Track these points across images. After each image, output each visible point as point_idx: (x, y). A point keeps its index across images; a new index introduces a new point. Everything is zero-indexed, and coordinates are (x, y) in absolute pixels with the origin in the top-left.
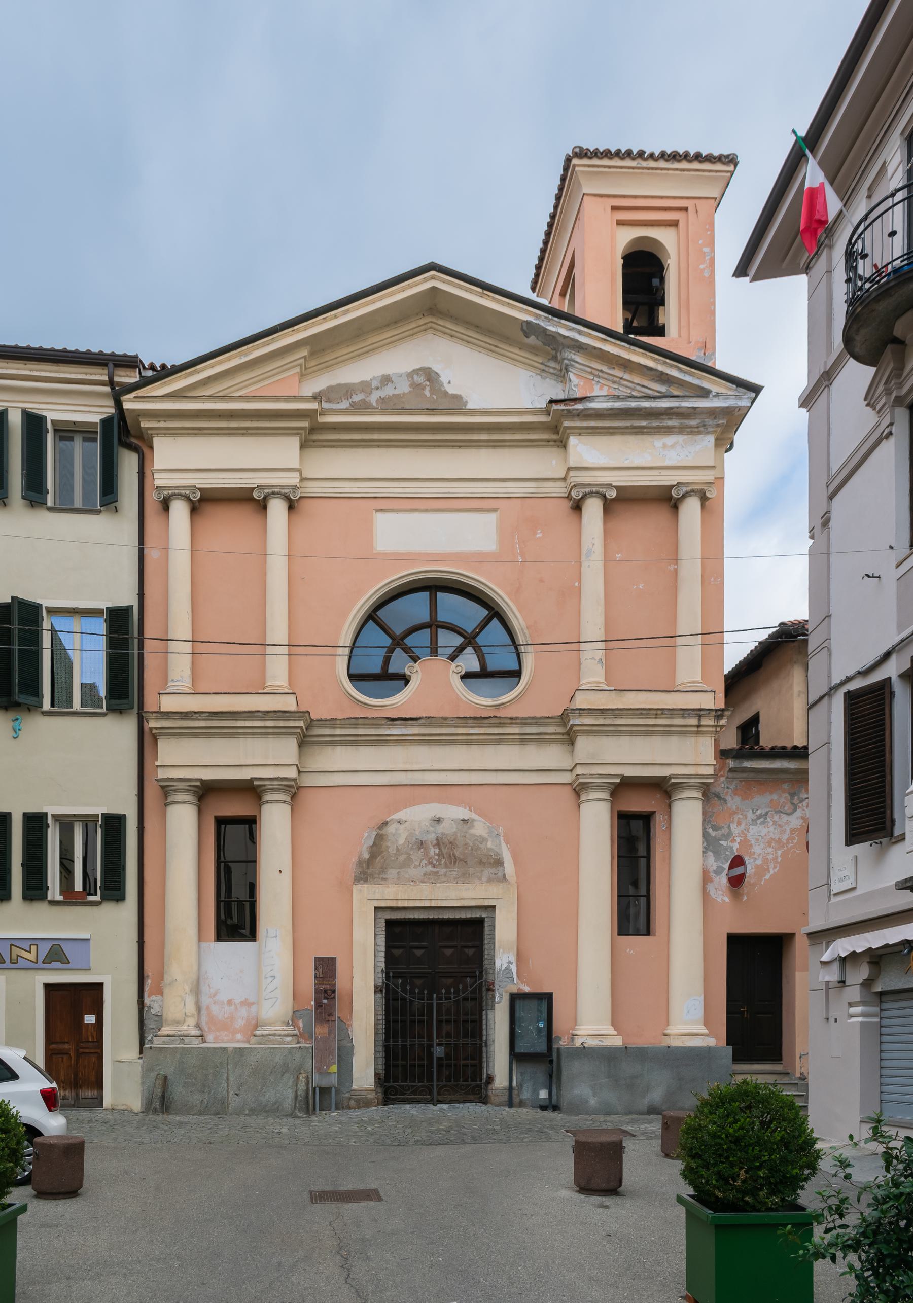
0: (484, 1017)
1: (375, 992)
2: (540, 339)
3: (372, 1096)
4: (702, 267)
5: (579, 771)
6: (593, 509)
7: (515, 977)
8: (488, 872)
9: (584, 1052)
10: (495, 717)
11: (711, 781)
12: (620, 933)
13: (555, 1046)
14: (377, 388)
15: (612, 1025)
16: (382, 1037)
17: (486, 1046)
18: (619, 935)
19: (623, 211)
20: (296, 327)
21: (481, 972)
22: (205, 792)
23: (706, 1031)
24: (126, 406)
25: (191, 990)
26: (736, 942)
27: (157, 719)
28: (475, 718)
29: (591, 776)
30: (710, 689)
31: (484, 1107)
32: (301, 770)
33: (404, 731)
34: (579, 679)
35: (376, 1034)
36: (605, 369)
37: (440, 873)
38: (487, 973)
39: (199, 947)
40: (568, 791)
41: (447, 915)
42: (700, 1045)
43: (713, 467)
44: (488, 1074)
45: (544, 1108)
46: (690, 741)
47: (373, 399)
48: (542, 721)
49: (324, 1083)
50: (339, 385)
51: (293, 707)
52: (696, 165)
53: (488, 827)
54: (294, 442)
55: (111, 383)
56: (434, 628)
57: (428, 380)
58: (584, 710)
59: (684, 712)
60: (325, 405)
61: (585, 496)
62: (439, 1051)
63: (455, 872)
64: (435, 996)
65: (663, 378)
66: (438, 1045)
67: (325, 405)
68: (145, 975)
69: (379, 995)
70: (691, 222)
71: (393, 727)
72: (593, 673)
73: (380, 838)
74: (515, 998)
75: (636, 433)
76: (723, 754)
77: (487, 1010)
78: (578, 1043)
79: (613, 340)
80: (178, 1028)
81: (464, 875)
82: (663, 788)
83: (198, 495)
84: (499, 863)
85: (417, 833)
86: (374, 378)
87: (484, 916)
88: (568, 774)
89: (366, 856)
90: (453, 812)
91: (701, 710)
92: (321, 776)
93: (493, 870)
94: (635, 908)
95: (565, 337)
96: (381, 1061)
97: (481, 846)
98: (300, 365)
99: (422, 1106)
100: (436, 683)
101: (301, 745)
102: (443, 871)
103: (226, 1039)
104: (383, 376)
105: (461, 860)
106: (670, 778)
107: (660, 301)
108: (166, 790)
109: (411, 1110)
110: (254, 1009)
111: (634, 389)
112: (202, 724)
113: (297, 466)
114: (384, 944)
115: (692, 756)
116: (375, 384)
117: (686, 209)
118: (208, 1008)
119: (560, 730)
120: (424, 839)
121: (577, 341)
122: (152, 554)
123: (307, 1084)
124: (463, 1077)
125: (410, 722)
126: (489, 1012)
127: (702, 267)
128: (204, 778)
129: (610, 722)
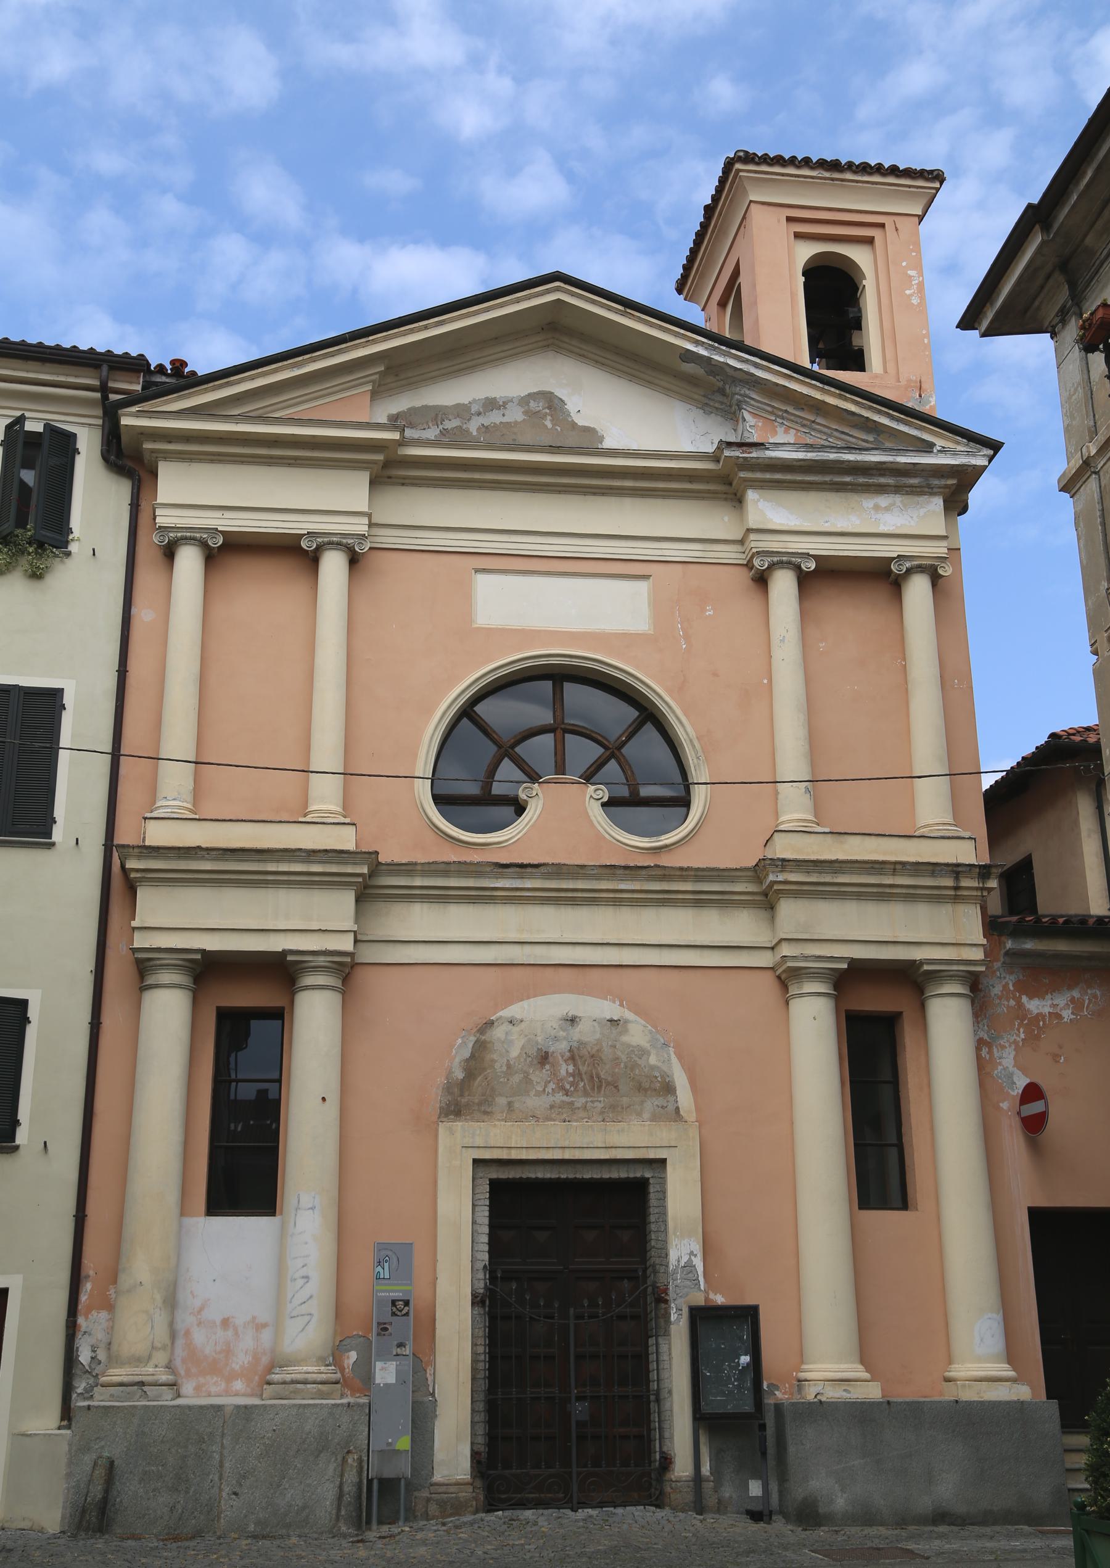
0: (652, 1349)
1: (473, 1304)
2: (710, 387)
3: (466, 1494)
4: (908, 292)
5: (786, 950)
6: (784, 584)
7: (701, 1279)
8: (651, 1104)
9: (819, 1410)
10: (657, 866)
11: (983, 969)
12: (862, 1206)
13: (769, 1401)
14: (479, 414)
15: (862, 1362)
16: (483, 1385)
17: (658, 1400)
18: (860, 1208)
19: (803, 227)
20: (371, 338)
21: (645, 1270)
22: (207, 970)
23: (1012, 1374)
24: (125, 421)
25: (164, 1302)
26: (1042, 1221)
27: (139, 857)
28: (626, 868)
29: (806, 958)
30: (967, 834)
31: (660, 1514)
32: (359, 937)
33: (518, 884)
34: (777, 815)
35: (473, 1379)
36: (790, 409)
37: (577, 1105)
38: (655, 1272)
39: (180, 1226)
40: (768, 979)
41: (588, 1174)
42: (1007, 1398)
43: (945, 538)
44: (662, 1452)
45: (756, 1516)
46: (945, 911)
47: (473, 427)
48: (726, 874)
49: (388, 1473)
50: (426, 407)
51: (351, 846)
52: (891, 180)
53: (651, 1032)
54: (363, 479)
55: (104, 389)
56: (559, 732)
57: (549, 408)
58: (789, 861)
59: (934, 868)
60: (409, 433)
61: (772, 567)
62: (579, 1410)
63: (600, 1102)
64: (572, 1311)
65: (868, 426)
66: (579, 1398)
67: (409, 433)
68: (83, 1274)
69: (477, 1310)
70: (889, 241)
71: (502, 876)
72: (795, 807)
73: (481, 1047)
74: (703, 1318)
75: (838, 491)
76: (992, 926)
77: (657, 1336)
78: (810, 1394)
79: (801, 378)
80: (137, 1370)
81: (613, 1107)
82: (911, 979)
83: (220, 541)
84: (668, 1089)
85: (539, 1039)
86: (474, 401)
87: (647, 1175)
88: (768, 954)
89: (459, 1075)
90: (595, 1008)
91: (958, 865)
92: (390, 948)
93: (660, 1101)
94: (881, 1168)
95: (736, 369)
96: (481, 1429)
97: (639, 1062)
98: (373, 382)
99: (553, 1513)
100: (564, 817)
101: (360, 900)
102: (580, 1101)
103: (214, 1389)
104: (487, 398)
105: (608, 1084)
106: (922, 963)
107: (857, 324)
108: (144, 967)
109: (541, 1520)
110: (266, 1336)
111: (830, 436)
112: (207, 866)
113: (366, 509)
114: (486, 1221)
115: (951, 933)
116: (474, 408)
117: (882, 226)
118: (187, 1333)
119: (751, 888)
120: (551, 1049)
121: (753, 375)
122: (143, 614)
123: (360, 1473)
124: (627, 1467)
125: (529, 870)
126: (660, 1340)
127: (908, 292)
128: (208, 948)
129: (826, 881)
